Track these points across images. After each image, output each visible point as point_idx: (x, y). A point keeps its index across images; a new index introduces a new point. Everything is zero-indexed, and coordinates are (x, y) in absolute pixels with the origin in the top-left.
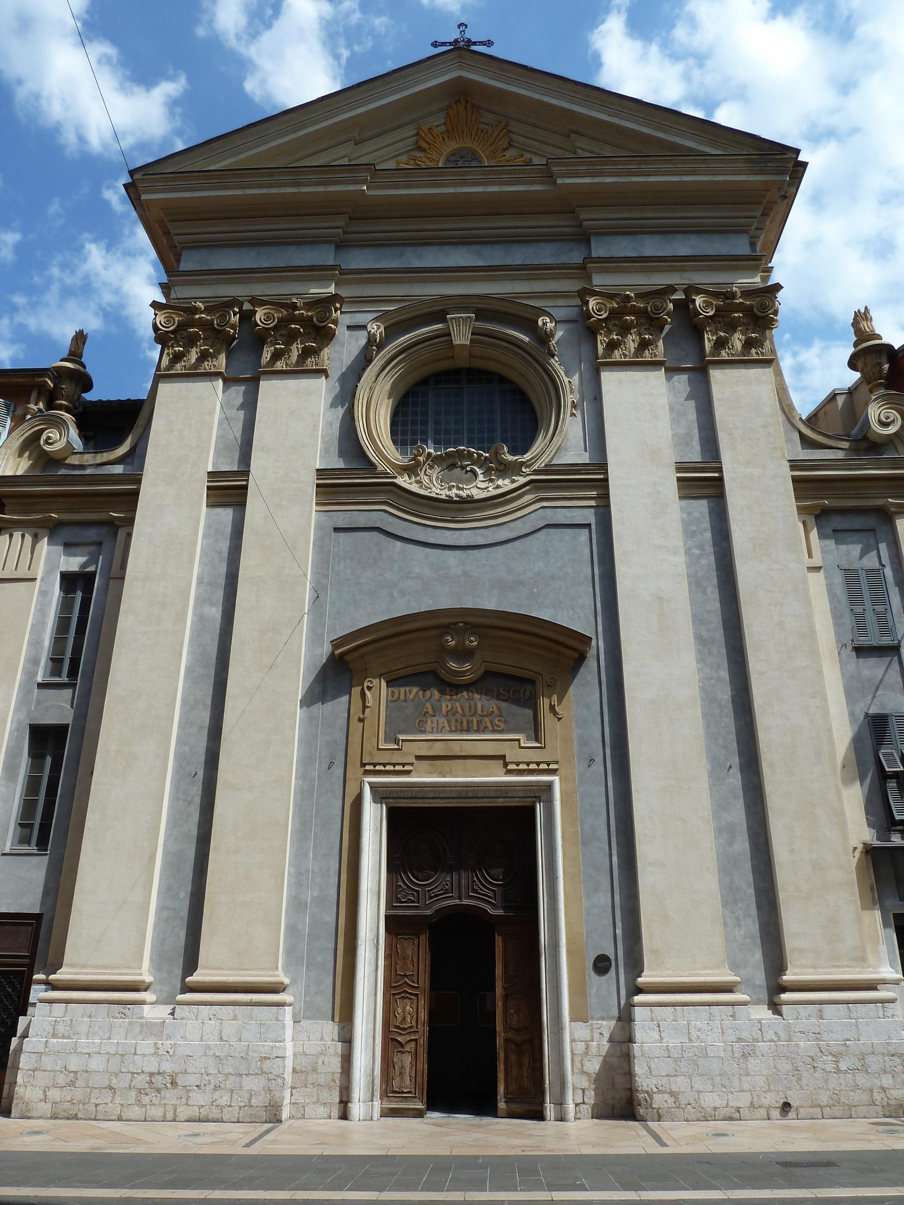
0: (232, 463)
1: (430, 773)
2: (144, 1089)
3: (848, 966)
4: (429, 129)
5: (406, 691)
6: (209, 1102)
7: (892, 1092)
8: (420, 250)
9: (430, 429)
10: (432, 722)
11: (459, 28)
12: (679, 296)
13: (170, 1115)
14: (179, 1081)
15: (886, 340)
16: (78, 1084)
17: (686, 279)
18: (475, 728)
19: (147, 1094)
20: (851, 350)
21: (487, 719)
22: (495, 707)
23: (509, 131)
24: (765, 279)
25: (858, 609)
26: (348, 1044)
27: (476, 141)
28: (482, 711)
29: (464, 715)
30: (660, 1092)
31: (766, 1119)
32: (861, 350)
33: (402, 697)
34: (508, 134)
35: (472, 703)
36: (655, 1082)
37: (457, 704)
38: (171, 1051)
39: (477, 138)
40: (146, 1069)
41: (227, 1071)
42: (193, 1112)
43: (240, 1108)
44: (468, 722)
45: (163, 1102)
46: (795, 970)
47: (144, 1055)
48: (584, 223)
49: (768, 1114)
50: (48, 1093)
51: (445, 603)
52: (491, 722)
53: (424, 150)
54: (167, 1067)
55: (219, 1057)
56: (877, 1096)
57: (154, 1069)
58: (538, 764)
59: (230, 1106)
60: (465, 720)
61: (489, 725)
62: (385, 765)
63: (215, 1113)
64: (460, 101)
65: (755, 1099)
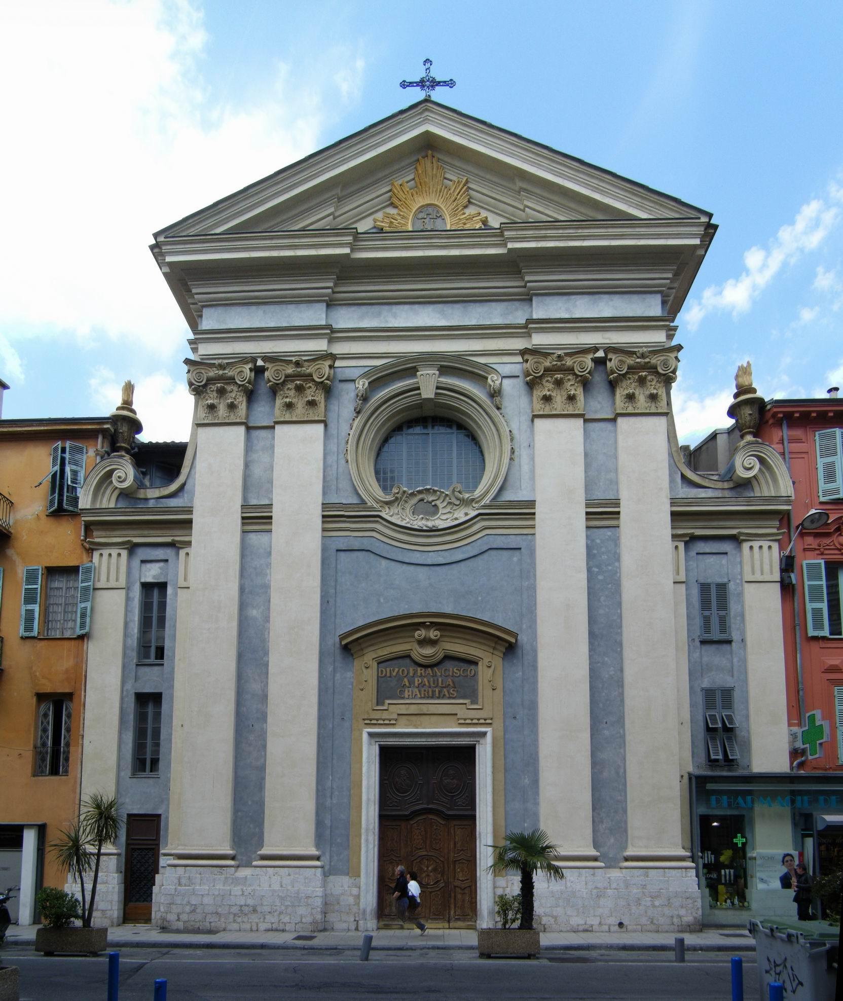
0: (258, 497)
1: (407, 726)
2: (238, 914)
3: (668, 847)
4: (401, 185)
5: (390, 670)
6: (277, 921)
7: (685, 918)
8: (395, 309)
9: (404, 450)
10: (408, 692)
11: (425, 65)
12: (600, 354)
13: (254, 928)
14: (259, 909)
15: (759, 394)
16: (198, 911)
17: (606, 339)
18: (437, 695)
19: (239, 917)
20: (731, 401)
21: (445, 690)
22: (450, 681)
23: (469, 188)
24: (670, 337)
25: (707, 613)
26: (96, 587)
27: (440, 197)
28: (442, 684)
29: (430, 687)
30: (546, 916)
31: (606, 932)
32: (741, 401)
33: (388, 674)
34: (468, 191)
35: (436, 679)
36: (543, 910)
37: (425, 679)
38: (252, 893)
39: (441, 195)
40: (238, 903)
41: (286, 904)
42: (269, 926)
43: (296, 924)
44: (433, 691)
45: (250, 921)
46: (635, 849)
47: (236, 896)
48: (528, 284)
49: (609, 929)
50: (181, 917)
51: (417, 608)
52: (448, 692)
53: (396, 207)
54: (250, 902)
55: (281, 896)
56: (675, 920)
57: (243, 903)
58: (479, 719)
59: (290, 923)
60: (430, 690)
61: (446, 693)
62: (377, 720)
63: (281, 927)
64: (427, 156)
65: (603, 920)
